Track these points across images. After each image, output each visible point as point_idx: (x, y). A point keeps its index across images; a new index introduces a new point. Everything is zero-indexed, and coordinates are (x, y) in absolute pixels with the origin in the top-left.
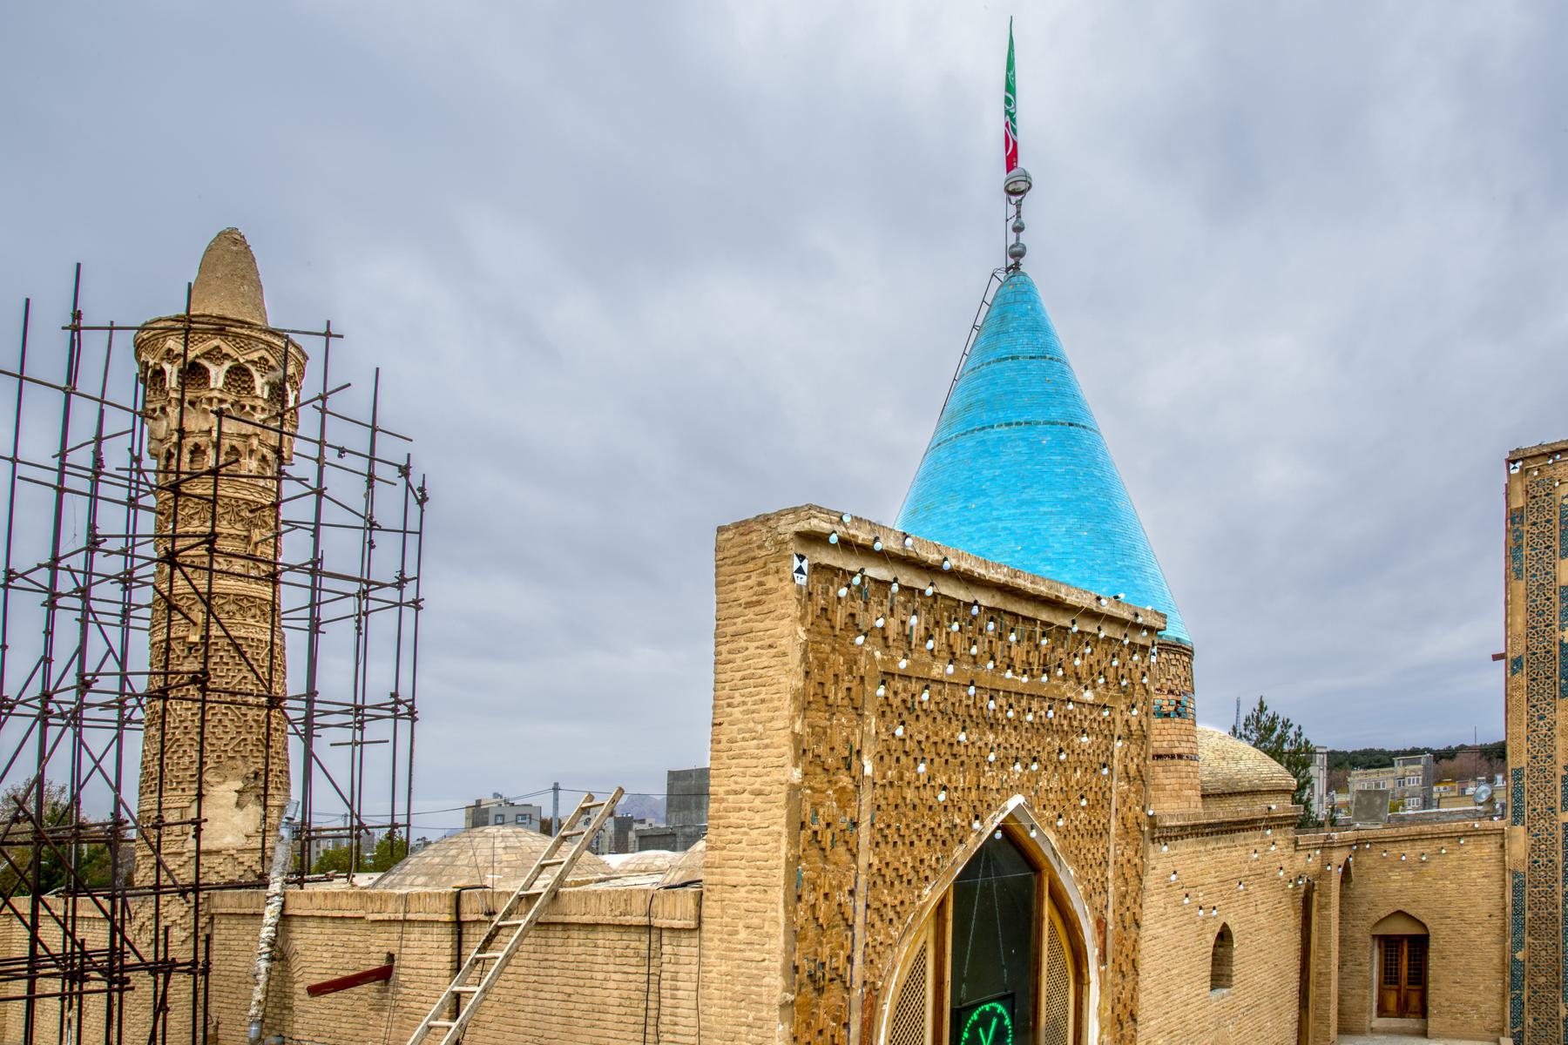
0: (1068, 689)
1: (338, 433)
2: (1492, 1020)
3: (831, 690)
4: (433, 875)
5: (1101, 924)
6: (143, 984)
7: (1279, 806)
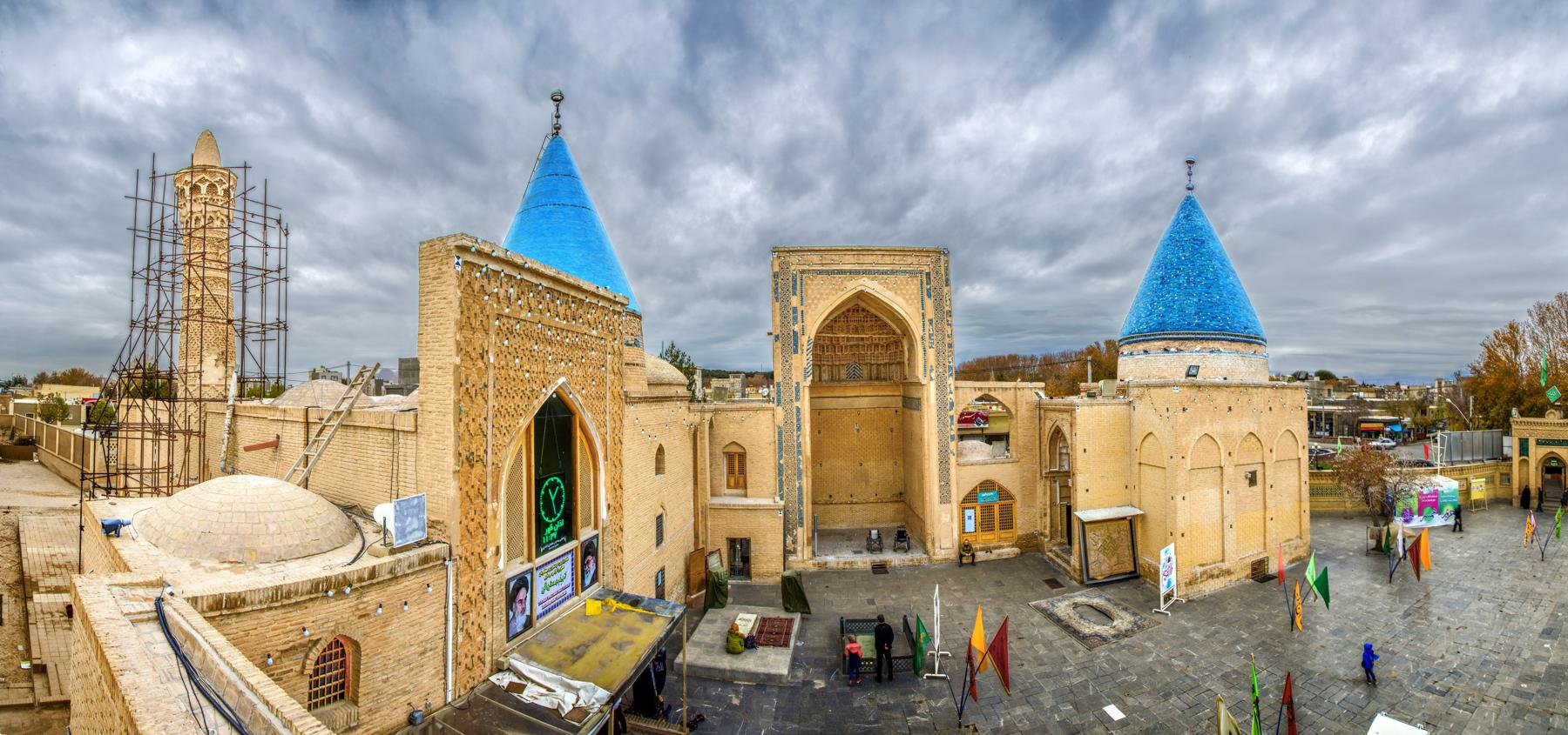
0: (585, 329)
1: (251, 208)
2: (772, 490)
3: (473, 320)
4: (296, 401)
5: (604, 442)
6: (180, 437)
7: (682, 391)
